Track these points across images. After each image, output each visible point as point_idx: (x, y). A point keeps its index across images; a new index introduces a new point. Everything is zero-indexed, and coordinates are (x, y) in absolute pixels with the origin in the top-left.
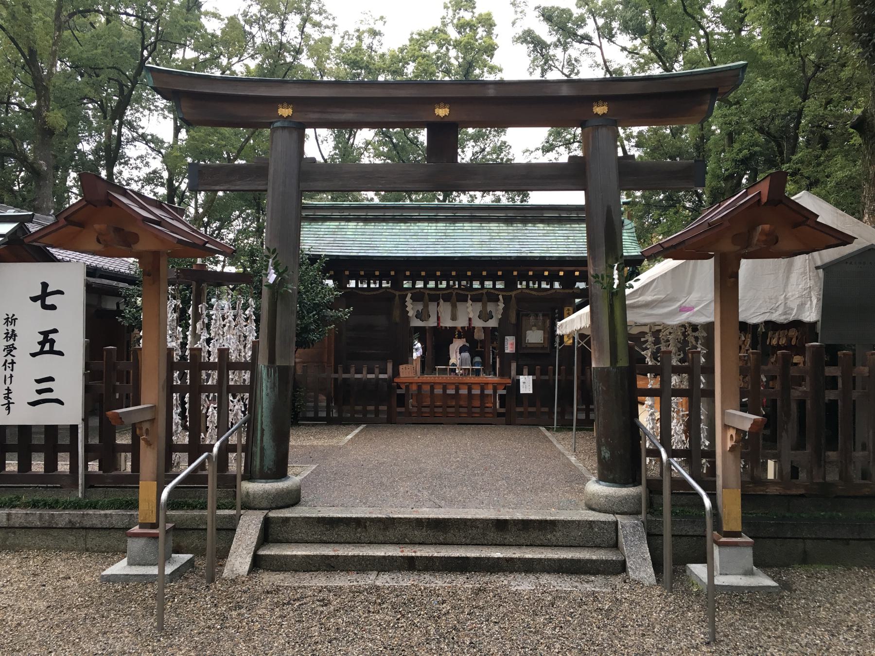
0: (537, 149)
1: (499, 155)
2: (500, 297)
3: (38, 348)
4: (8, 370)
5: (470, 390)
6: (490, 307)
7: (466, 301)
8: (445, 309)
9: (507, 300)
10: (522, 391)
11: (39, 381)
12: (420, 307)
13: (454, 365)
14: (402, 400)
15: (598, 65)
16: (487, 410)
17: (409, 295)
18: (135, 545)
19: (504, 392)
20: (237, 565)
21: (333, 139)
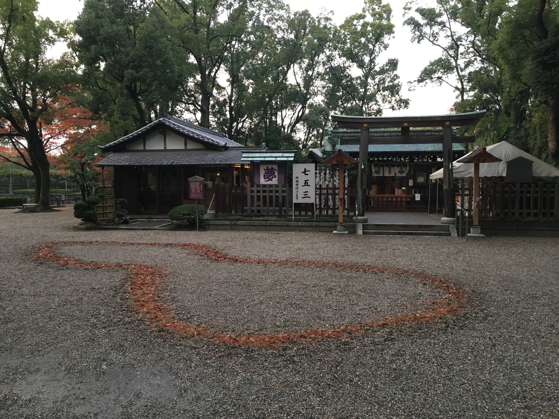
0: (415, 81)
3: (304, 184)
5: (397, 199)
6: (404, 169)
8: (387, 169)
9: (410, 166)
10: (416, 199)
12: (377, 169)
18: (338, 227)
19: (409, 200)
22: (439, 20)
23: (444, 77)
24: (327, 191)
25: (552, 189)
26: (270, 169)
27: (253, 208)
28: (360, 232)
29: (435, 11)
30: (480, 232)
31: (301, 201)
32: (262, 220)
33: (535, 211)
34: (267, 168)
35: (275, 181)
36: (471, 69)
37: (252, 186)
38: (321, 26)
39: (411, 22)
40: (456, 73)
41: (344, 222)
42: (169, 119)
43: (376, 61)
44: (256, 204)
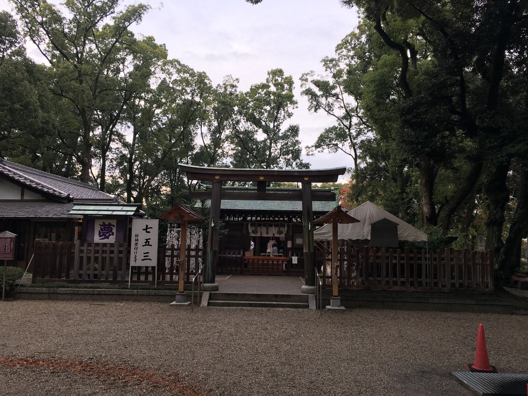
1: (294, 148)
2: (286, 225)
3: (144, 244)
4: (136, 250)
5: (273, 262)
6: (282, 229)
7: (272, 226)
8: (264, 229)
9: (288, 226)
10: (293, 263)
11: (144, 253)
12: (254, 228)
13: (269, 253)
14: (246, 265)
15: (342, 107)
16: (279, 270)
17: (250, 224)
18: (178, 297)
19: (286, 263)
20: (204, 304)
21: (210, 135)
22: (333, 92)
23: (340, 145)
24: (172, 253)
25: (419, 256)
26: (107, 225)
27: (81, 272)
28: (204, 303)
29: (329, 84)
30: (340, 304)
31: (139, 263)
32: (90, 288)
33: (402, 279)
34: (104, 223)
35: (112, 239)
36: (362, 138)
37: (82, 245)
38: (228, 92)
39: (308, 92)
40: (349, 141)
41: (185, 290)
42: (5, 165)
43: (281, 127)
44: (85, 267)
